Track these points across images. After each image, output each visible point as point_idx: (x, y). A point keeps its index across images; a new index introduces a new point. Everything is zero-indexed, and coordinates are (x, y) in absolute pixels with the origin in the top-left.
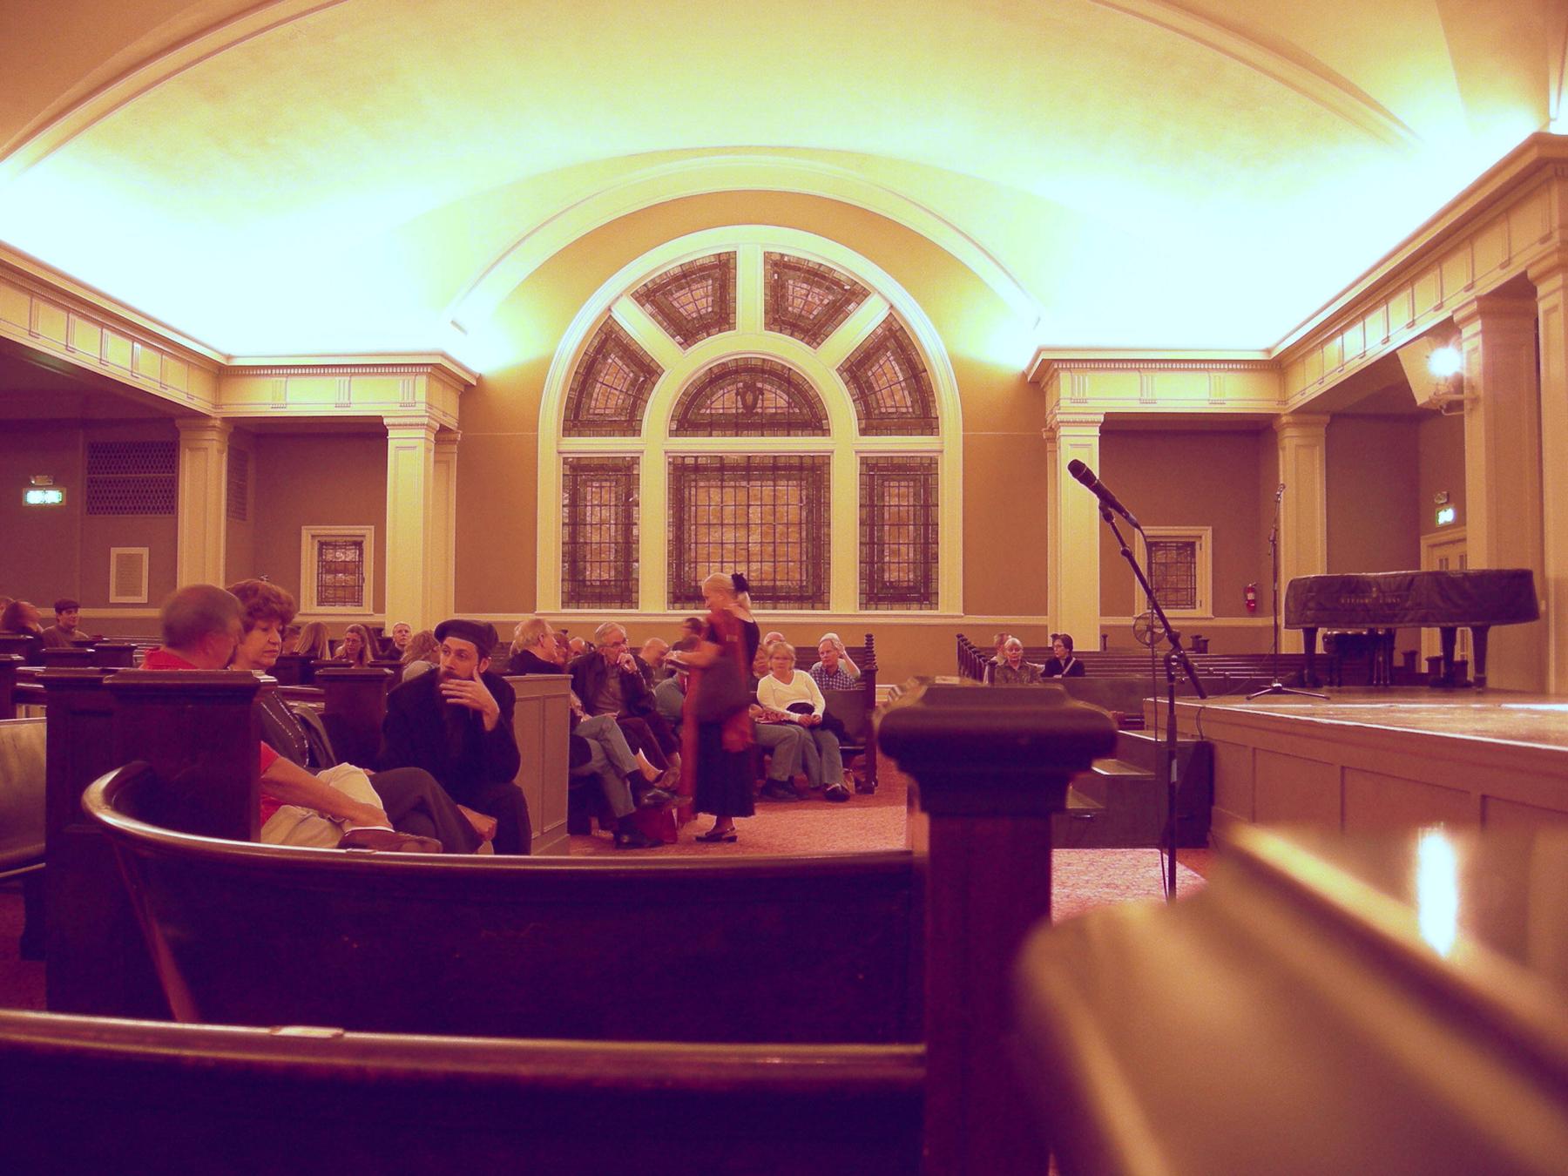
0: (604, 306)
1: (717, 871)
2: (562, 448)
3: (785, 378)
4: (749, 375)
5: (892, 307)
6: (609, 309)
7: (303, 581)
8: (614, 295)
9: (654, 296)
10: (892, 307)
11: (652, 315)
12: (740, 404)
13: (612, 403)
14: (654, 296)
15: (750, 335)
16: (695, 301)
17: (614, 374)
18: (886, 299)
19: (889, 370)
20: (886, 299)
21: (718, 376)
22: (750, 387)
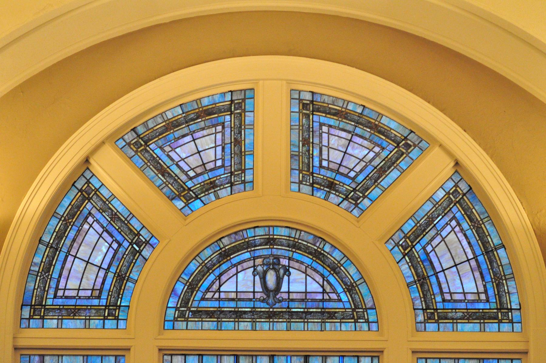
0: (85, 155)
1: (493, 205)
2: (22, 343)
3: (317, 253)
4: (271, 247)
5: (457, 164)
6: (87, 161)
7: (421, 100)
8: (95, 141)
9: (143, 143)
10: (457, 164)
11: (142, 170)
12: (259, 288)
13: (87, 284)
14: (143, 143)
15: (273, 195)
16: (200, 150)
17: (94, 248)
18: (449, 153)
19: (451, 248)
20: (449, 153)
21: (227, 252)
22: (274, 264)
